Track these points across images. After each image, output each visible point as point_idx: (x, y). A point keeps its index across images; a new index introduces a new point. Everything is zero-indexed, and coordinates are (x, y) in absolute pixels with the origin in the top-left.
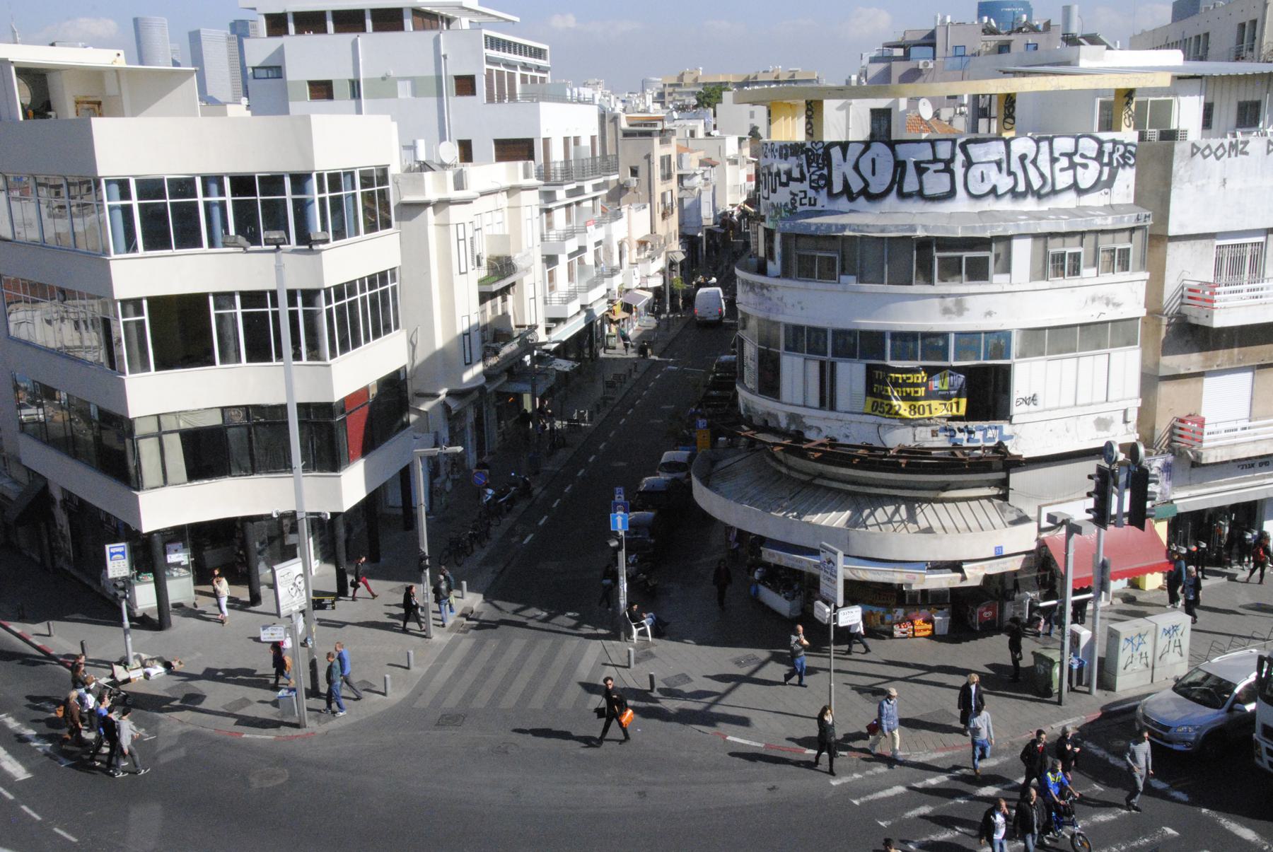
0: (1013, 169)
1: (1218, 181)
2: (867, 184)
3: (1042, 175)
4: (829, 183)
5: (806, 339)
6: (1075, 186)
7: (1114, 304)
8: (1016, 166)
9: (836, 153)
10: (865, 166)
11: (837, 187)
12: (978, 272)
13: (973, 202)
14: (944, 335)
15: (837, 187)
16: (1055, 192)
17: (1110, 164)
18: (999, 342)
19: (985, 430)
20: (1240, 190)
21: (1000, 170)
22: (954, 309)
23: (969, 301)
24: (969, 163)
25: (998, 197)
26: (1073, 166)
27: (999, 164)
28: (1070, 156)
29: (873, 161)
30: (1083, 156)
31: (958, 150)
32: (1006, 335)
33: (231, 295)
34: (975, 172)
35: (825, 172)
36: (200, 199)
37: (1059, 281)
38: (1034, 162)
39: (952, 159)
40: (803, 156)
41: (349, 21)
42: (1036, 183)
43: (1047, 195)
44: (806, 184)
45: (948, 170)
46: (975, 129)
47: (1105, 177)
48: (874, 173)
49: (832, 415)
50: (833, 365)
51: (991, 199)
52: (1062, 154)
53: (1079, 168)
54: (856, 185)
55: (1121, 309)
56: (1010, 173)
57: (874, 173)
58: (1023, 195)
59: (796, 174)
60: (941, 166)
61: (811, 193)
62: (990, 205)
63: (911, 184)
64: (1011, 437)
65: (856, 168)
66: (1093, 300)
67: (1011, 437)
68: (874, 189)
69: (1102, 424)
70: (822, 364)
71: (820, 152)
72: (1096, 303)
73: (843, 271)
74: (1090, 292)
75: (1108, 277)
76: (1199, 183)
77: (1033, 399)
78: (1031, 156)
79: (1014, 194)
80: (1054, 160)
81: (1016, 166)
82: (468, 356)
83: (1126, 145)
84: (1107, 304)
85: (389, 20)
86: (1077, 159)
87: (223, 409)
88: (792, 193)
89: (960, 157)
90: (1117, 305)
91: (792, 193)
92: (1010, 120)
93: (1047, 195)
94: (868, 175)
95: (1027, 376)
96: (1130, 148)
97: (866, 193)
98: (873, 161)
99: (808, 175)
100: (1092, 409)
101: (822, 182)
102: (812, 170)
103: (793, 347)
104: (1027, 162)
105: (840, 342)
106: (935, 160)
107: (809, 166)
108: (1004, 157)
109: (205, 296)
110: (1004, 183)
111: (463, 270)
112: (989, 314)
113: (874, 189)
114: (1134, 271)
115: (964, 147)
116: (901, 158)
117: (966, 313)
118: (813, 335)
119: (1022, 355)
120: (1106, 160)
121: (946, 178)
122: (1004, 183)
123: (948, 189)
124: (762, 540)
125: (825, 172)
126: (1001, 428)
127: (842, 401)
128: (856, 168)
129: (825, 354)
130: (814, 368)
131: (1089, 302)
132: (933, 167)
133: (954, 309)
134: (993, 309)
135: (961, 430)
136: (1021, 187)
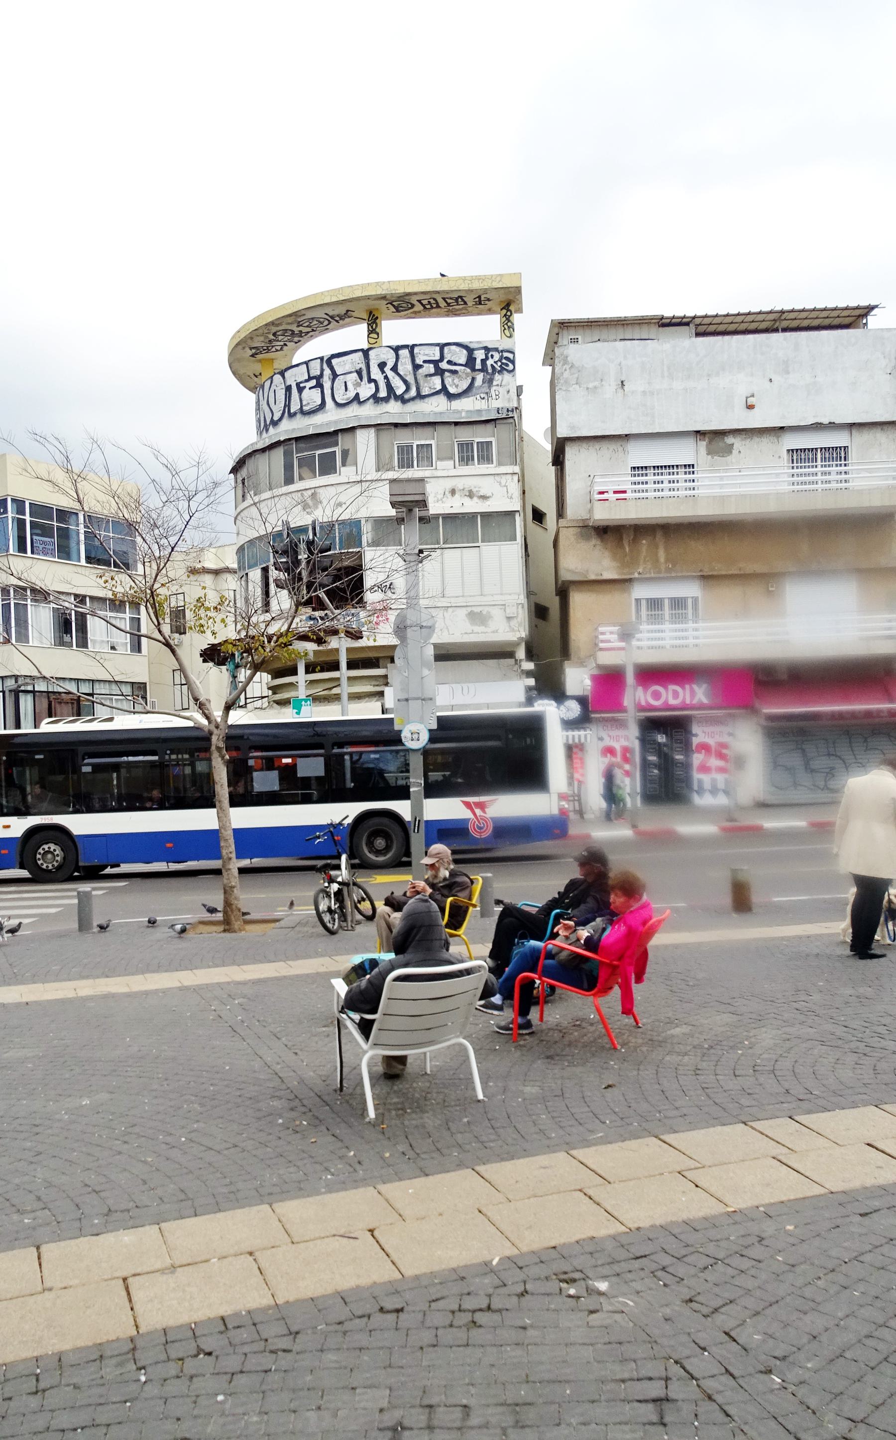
1: (613, 384)
3: (405, 382)
6: (444, 390)
8: (376, 374)
12: (328, 466)
17: (484, 369)
18: (352, 531)
20: (644, 392)
21: (361, 378)
23: (323, 494)
24: (335, 375)
25: (361, 403)
26: (440, 372)
27: (359, 373)
28: (436, 363)
30: (449, 362)
31: (325, 366)
32: (356, 524)
34: (339, 382)
38: (395, 369)
39: (321, 375)
42: (400, 388)
43: (413, 399)
45: (319, 385)
51: (355, 406)
52: (425, 362)
53: (447, 374)
55: (488, 503)
56: (370, 380)
58: (386, 400)
60: (313, 383)
62: (354, 411)
69: (477, 618)
74: (449, 484)
76: (591, 385)
78: (390, 364)
79: (375, 398)
80: (416, 367)
81: (376, 374)
86: (444, 365)
89: (327, 372)
90: (484, 498)
92: (375, 336)
93: (413, 399)
104: (387, 369)
106: (310, 378)
114: (500, 464)
115: (329, 362)
119: (375, 543)
120: (478, 366)
121: (316, 393)
122: (366, 390)
123: (319, 402)
131: (448, 495)
136: (383, 393)
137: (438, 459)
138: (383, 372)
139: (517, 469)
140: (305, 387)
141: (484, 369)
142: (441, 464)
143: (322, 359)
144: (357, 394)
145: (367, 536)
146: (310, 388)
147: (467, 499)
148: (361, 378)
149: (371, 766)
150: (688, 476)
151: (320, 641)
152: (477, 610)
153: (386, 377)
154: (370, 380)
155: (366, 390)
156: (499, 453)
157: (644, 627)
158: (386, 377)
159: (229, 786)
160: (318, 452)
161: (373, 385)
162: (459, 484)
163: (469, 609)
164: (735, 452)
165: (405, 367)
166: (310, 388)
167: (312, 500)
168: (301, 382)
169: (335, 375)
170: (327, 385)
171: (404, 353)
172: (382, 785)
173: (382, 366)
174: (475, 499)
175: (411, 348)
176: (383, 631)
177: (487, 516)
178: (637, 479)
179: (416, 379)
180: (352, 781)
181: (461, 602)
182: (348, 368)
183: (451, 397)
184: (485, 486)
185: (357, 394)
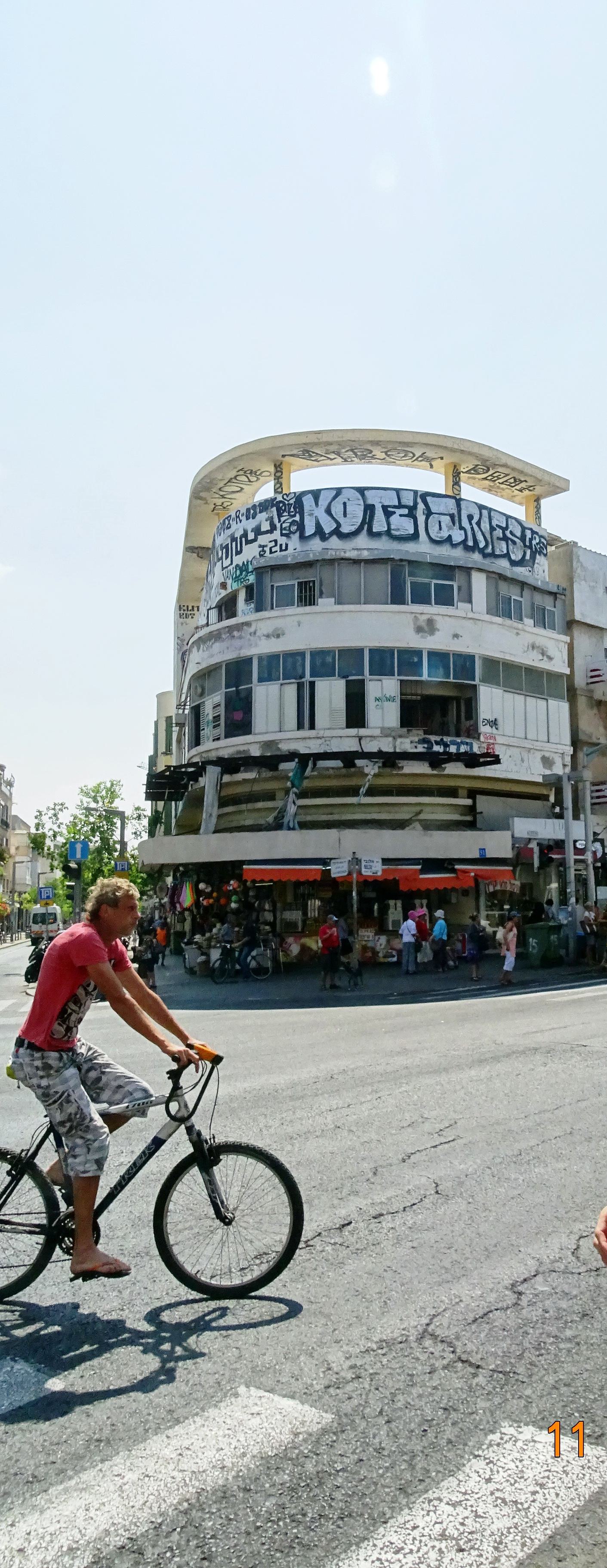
0: (463, 525)
2: (339, 525)
4: (301, 527)
5: (278, 667)
6: (507, 555)
8: (465, 523)
9: (308, 501)
10: (337, 509)
11: (310, 529)
12: (445, 598)
13: (433, 546)
14: (418, 653)
15: (310, 529)
16: (493, 555)
21: (454, 524)
22: (426, 628)
23: (440, 622)
24: (429, 513)
27: (452, 516)
29: (345, 504)
31: (419, 500)
35: (297, 518)
38: (479, 524)
40: (274, 509)
44: (276, 534)
46: (164, 888)
47: (528, 557)
48: (345, 515)
49: (312, 733)
50: (312, 685)
54: (328, 526)
56: (461, 528)
57: (345, 515)
59: (266, 527)
60: (406, 511)
61: (282, 540)
63: (379, 524)
65: (328, 511)
68: (345, 529)
70: (300, 687)
71: (292, 502)
73: (321, 596)
80: (492, 529)
81: (465, 523)
83: (541, 537)
88: (260, 546)
89: (421, 506)
90: (550, 658)
91: (260, 546)
94: (341, 520)
96: (543, 540)
97: (337, 532)
98: (345, 504)
99: (278, 525)
101: (294, 528)
102: (283, 519)
103: (267, 676)
105: (318, 662)
106: (400, 506)
107: (280, 516)
108: (455, 512)
110: (458, 536)
112: (456, 636)
113: (345, 529)
114: (559, 633)
116: (370, 502)
117: (437, 633)
118: (290, 660)
124: (243, 862)
125: (297, 518)
128: (328, 511)
129: (302, 676)
130: (291, 691)
131: (530, 648)
132: (399, 511)
133: (426, 628)
135: (437, 743)
138: (471, 524)
139: (568, 639)
140: (394, 513)
141: (530, 547)
143: (416, 492)
144: (450, 536)
146: (401, 515)
148: (454, 524)
152: (547, 755)
153: (472, 529)
154: (461, 528)
155: (458, 536)
158: (472, 529)
159: (517, 947)
160: (434, 581)
161: (462, 532)
165: (485, 526)
166: (401, 515)
167: (429, 627)
168: (389, 506)
169: (429, 513)
170: (421, 519)
171: (485, 513)
173: (470, 518)
175: (361, 491)
179: (492, 537)
180: (389, 905)
182: (442, 509)
183: (342, 536)
185: (450, 536)
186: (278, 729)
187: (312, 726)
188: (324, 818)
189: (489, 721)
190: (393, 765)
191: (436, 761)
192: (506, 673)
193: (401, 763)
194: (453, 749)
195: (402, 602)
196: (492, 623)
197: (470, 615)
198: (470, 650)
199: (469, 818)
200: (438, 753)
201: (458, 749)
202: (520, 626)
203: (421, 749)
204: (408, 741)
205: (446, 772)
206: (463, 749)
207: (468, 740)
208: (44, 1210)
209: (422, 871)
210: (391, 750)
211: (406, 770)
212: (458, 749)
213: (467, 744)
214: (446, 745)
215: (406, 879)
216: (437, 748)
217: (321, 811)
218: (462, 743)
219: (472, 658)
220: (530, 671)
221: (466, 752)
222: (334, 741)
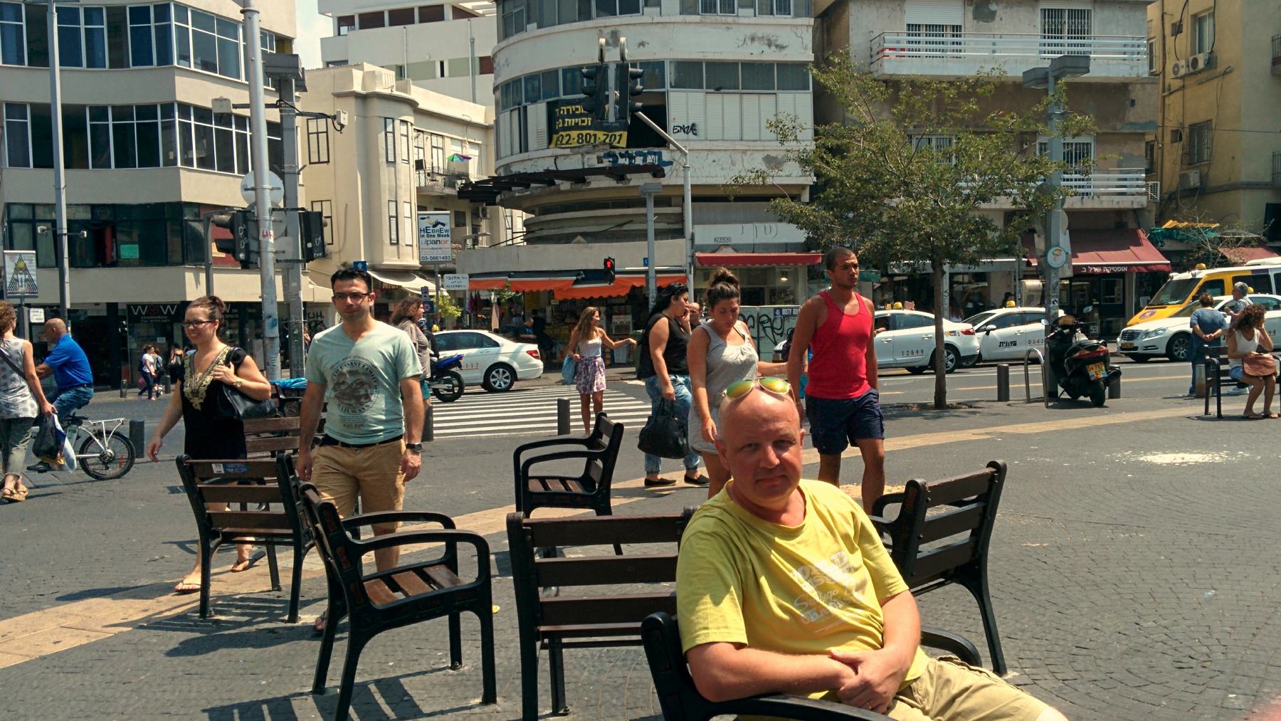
7: (777, 46)
19: (645, 156)
33: (105, 109)
36: (82, 27)
37: (710, 17)
41: (402, 17)
50: (525, 108)
64: (670, 163)
66: (753, 39)
67: (670, 163)
72: (756, 43)
73: (529, 22)
74: (750, 31)
75: (766, 19)
77: (693, 129)
82: (394, 237)
84: (769, 45)
85: (433, 14)
87: (93, 207)
90: (781, 47)
95: (683, 105)
100: (759, 145)
109: (84, 107)
111: (391, 159)
112: (642, 44)
114: (797, 15)
119: (678, 85)
126: (660, 154)
127: (532, 145)
134: (645, 40)
135: (622, 156)
137: (740, 6)
142: (742, 12)
145: (669, 75)
147: (766, 48)
149: (803, 401)
150: (956, 39)
151: (621, 178)
156: (795, 6)
157: (467, 288)
162: (760, 32)
163: (766, 153)
164: (997, 18)
172: (498, 198)
174: (773, 48)
176: (756, 110)
177: (783, 66)
178: (911, 38)
181: (759, 145)
184: (784, 37)
186: (738, 137)
187: (527, 150)
188: (553, 232)
189: (683, 128)
190: (583, 181)
191: (618, 173)
192: (693, 74)
193: (589, 178)
194: (639, 161)
195: (589, 17)
196: (686, 23)
197: (657, 19)
198: (659, 56)
199: (677, 226)
200: (623, 165)
201: (645, 160)
202: (730, 20)
203: (606, 163)
204: (594, 156)
205: (632, 184)
206: (650, 159)
207: (656, 150)
208: (198, 537)
209: (576, 282)
210: (580, 167)
211: (594, 185)
212: (645, 160)
213: (655, 154)
214: (631, 157)
215: (560, 289)
216: (621, 161)
217: (552, 225)
218: (650, 153)
219: (660, 64)
220: (749, 66)
221: (653, 164)
222: (540, 161)
